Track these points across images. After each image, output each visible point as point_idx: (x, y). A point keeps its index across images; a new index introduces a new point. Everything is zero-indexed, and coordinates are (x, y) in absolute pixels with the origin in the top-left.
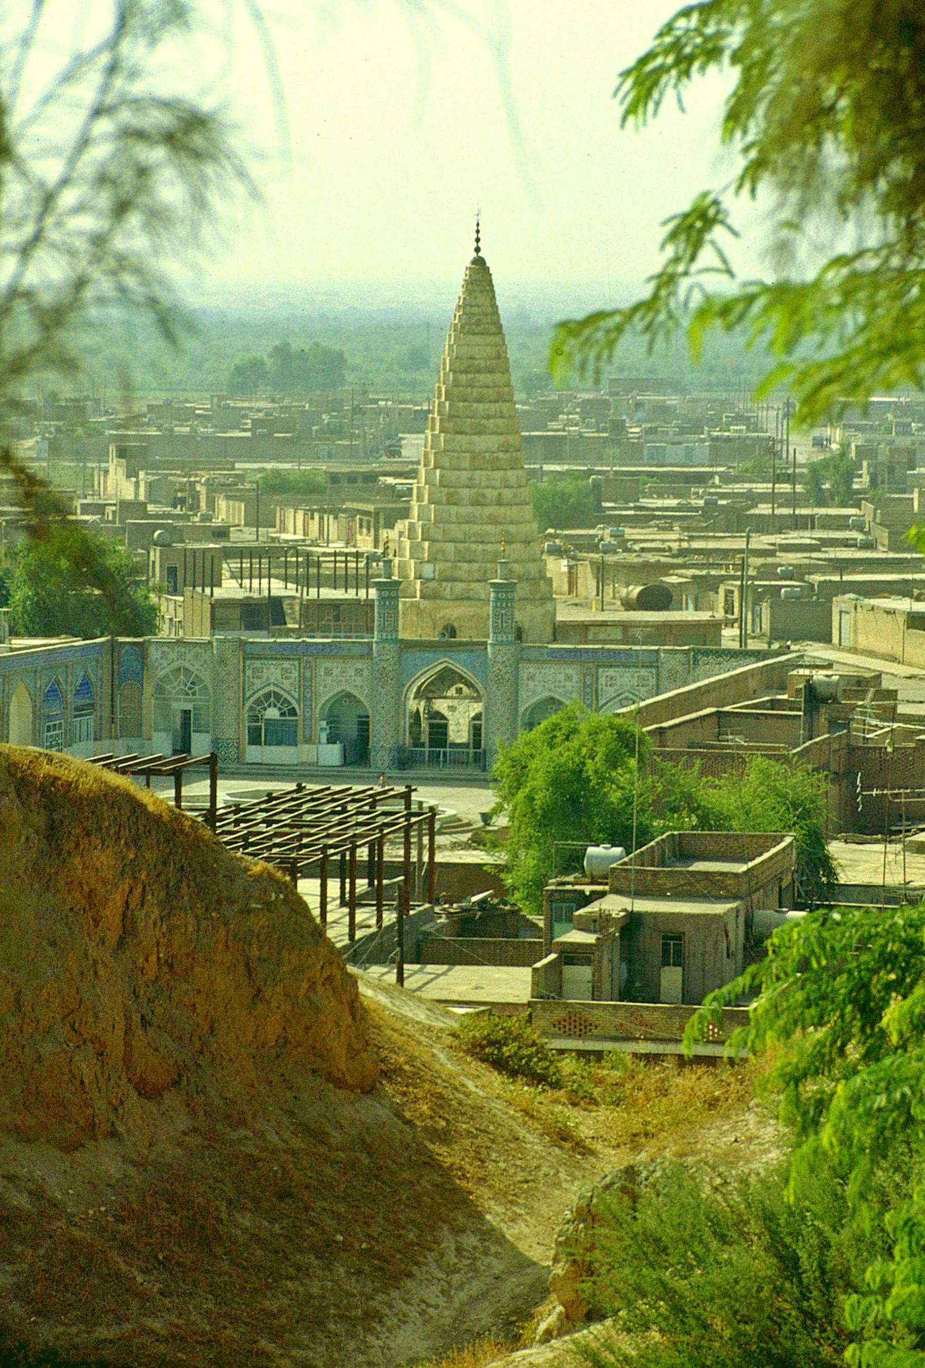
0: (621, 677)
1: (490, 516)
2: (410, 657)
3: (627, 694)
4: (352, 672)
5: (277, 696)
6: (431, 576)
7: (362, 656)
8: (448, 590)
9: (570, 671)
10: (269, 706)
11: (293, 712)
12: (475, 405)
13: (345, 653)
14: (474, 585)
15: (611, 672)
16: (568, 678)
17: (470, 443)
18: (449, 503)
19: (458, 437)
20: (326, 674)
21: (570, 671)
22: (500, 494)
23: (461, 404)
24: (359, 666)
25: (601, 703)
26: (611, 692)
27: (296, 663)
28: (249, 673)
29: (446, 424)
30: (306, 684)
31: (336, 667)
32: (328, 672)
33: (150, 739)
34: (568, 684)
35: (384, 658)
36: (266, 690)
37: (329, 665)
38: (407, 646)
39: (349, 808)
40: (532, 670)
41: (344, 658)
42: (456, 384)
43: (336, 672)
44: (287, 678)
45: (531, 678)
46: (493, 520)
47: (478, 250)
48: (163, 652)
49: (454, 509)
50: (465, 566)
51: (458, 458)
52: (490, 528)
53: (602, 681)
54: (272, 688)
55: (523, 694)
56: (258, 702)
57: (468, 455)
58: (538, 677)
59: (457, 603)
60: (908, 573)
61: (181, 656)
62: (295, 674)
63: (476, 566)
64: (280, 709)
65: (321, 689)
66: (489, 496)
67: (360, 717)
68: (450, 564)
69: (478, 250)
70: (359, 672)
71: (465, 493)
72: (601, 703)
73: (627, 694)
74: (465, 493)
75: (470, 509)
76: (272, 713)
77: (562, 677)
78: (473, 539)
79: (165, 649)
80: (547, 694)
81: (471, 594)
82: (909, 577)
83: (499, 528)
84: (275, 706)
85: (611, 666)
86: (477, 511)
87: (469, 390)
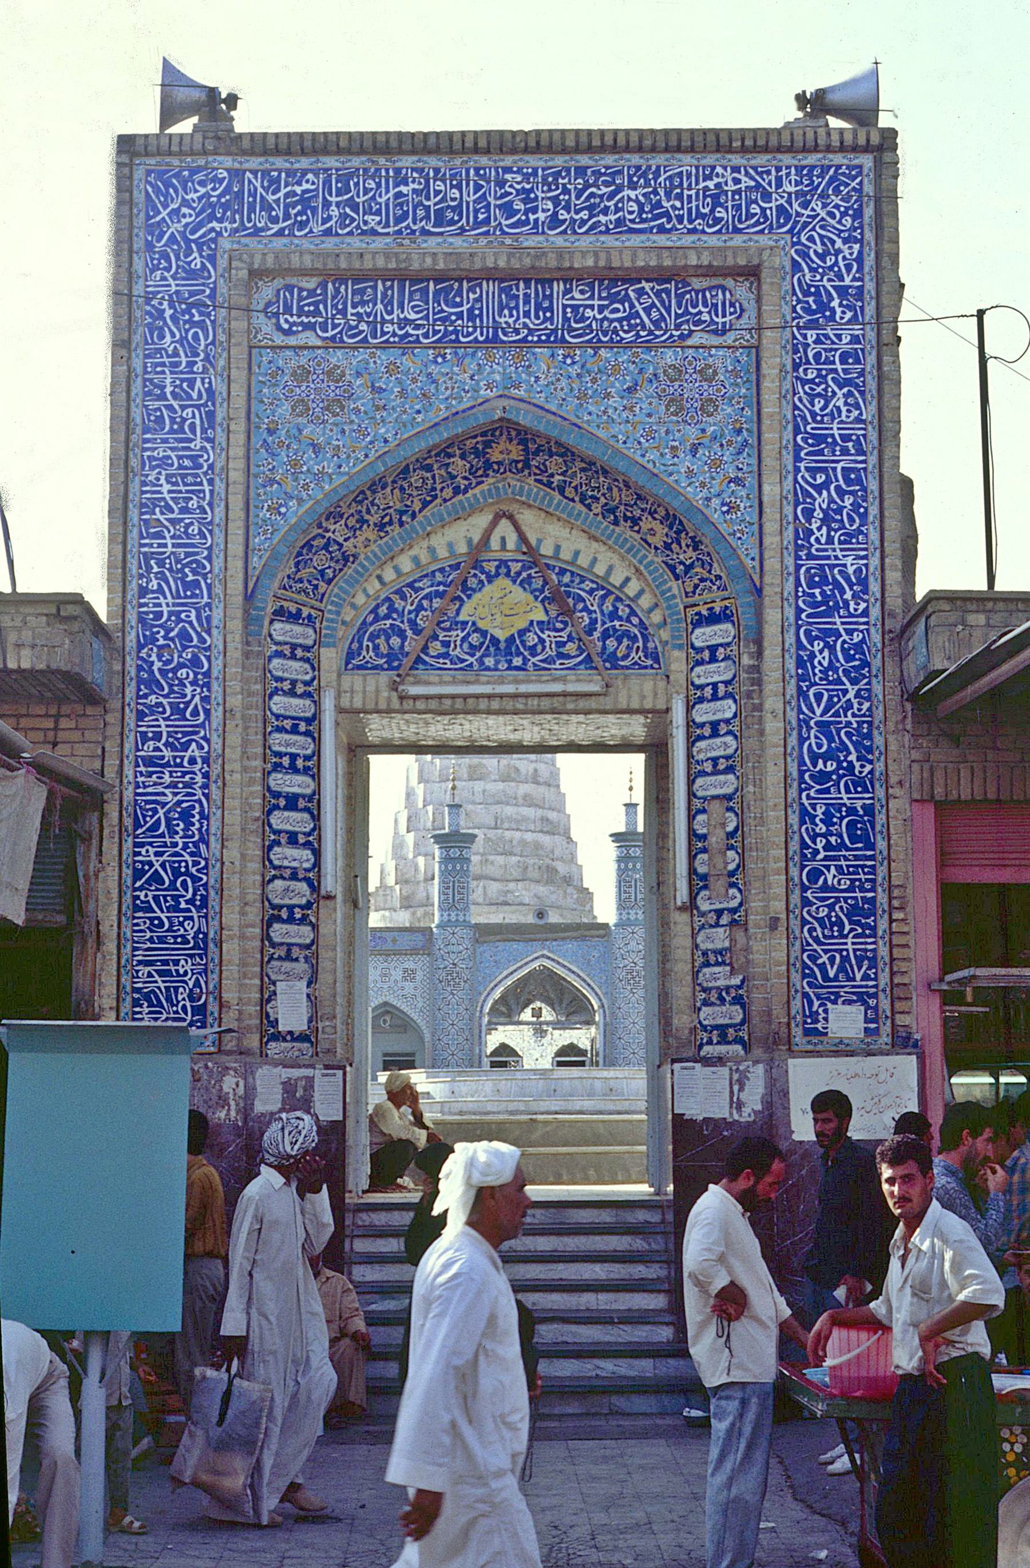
1: (526, 797)
2: (487, 951)
4: (397, 974)
7: (414, 952)
8: (480, 890)
13: (389, 946)
14: (512, 886)
22: (536, 770)
24: (410, 965)
35: (455, 948)
38: (485, 933)
46: (529, 801)
49: (479, 786)
50: (500, 860)
52: (530, 812)
59: (494, 908)
60: (665, 1083)
63: (514, 859)
66: (523, 771)
67: (385, 1055)
70: (409, 975)
75: (501, 786)
78: (506, 825)
81: (510, 898)
82: (1003, 971)
83: (540, 812)
86: (510, 787)
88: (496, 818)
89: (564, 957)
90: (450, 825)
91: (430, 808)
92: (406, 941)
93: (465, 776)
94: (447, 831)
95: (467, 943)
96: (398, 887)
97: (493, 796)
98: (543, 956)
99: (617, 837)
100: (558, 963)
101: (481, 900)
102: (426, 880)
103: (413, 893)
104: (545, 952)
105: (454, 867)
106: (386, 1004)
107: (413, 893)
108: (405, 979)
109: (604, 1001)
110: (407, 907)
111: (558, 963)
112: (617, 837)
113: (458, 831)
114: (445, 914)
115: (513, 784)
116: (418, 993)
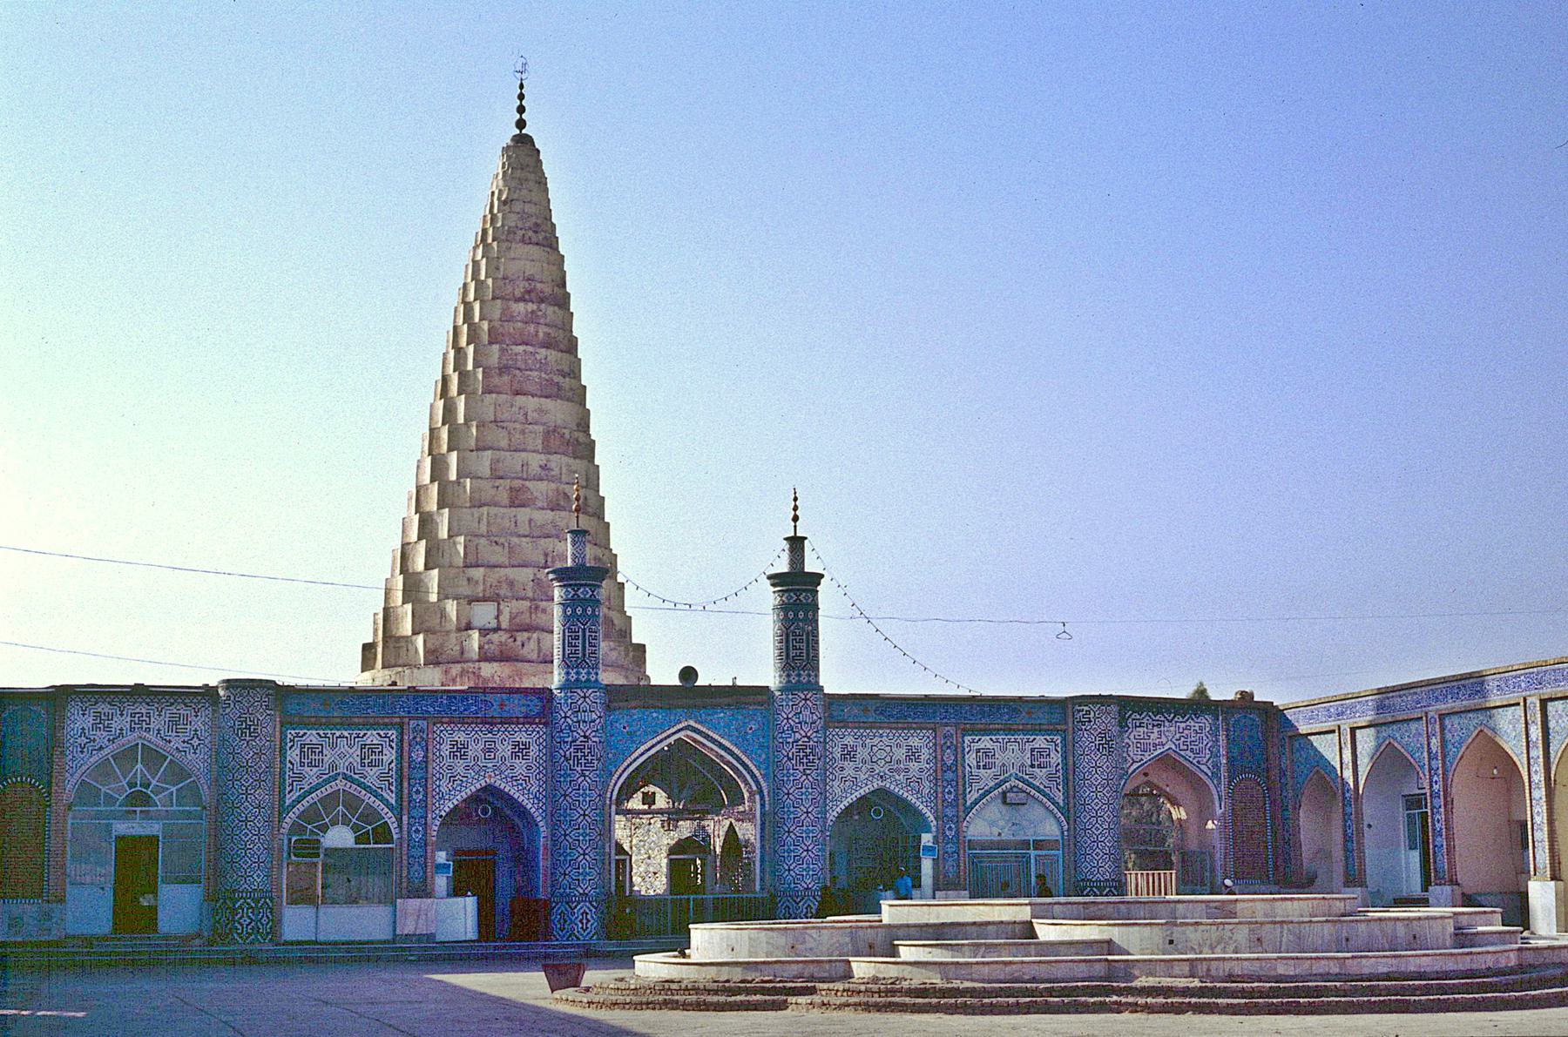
0: (1004, 750)
2: (621, 720)
3: (1014, 782)
4: (505, 749)
5: (352, 803)
6: (494, 624)
7: (528, 720)
8: (532, 645)
9: (915, 742)
10: (334, 823)
11: (383, 834)
12: (543, 351)
13: (495, 711)
15: (986, 742)
16: (913, 755)
17: (540, 410)
18: (513, 504)
19: (520, 400)
20: (453, 755)
21: (915, 742)
23: (520, 348)
24: (521, 737)
25: (971, 798)
26: (987, 777)
27: (393, 734)
28: (293, 755)
29: (496, 380)
30: (412, 776)
31: (474, 740)
32: (459, 751)
33: (61, 901)
34: (914, 766)
36: (328, 790)
37: (460, 737)
39: (907, 953)
40: (849, 740)
41: (490, 722)
42: (507, 317)
43: (475, 749)
44: (370, 765)
45: (849, 754)
47: (521, 124)
48: (98, 715)
49: (523, 514)
51: (523, 432)
53: (971, 759)
54: (340, 784)
55: (836, 787)
56: (310, 815)
57: (540, 428)
58: (862, 753)
61: (138, 723)
62: (390, 755)
64: (355, 829)
65: (444, 786)
68: (527, 603)
69: (521, 124)
70: (520, 750)
71: (540, 489)
72: (971, 798)
73: (1014, 782)
74: (540, 489)
75: (550, 515)
76: (340, 837)
77: (900, 753)
79: (104, 708)
80: (877, 784)
84: (346, 822)
85: (986, 731)
87: (532, 328)
88: (546, 555)
89: (715, 728)
90: (574, 557)
91: (461, 539)
92: (517, 707)
93: (506, 502)
94: (570, 563)
95: (599, 711)
96: (420, 639)
97: (542, 526)
98: (687, 728)
99: (776, 579)
100: (707, 737)
101: (534, 656)
102: (459, 630)
103: (442, 645)
104: (692, 723)
105: (585, 610)
106: (490, 790)
107: (442, 645)
108: (514, 755)
109: (764, 784)
110: (437, 664)
111: (707, 737)
112: (776, 579)
113: (583, 565)
114: (573, 672)
115: (563, 514)
116: (924, 775)
